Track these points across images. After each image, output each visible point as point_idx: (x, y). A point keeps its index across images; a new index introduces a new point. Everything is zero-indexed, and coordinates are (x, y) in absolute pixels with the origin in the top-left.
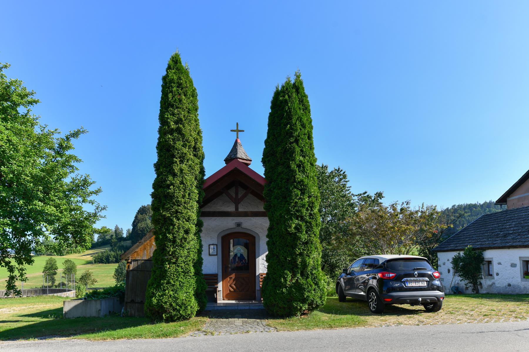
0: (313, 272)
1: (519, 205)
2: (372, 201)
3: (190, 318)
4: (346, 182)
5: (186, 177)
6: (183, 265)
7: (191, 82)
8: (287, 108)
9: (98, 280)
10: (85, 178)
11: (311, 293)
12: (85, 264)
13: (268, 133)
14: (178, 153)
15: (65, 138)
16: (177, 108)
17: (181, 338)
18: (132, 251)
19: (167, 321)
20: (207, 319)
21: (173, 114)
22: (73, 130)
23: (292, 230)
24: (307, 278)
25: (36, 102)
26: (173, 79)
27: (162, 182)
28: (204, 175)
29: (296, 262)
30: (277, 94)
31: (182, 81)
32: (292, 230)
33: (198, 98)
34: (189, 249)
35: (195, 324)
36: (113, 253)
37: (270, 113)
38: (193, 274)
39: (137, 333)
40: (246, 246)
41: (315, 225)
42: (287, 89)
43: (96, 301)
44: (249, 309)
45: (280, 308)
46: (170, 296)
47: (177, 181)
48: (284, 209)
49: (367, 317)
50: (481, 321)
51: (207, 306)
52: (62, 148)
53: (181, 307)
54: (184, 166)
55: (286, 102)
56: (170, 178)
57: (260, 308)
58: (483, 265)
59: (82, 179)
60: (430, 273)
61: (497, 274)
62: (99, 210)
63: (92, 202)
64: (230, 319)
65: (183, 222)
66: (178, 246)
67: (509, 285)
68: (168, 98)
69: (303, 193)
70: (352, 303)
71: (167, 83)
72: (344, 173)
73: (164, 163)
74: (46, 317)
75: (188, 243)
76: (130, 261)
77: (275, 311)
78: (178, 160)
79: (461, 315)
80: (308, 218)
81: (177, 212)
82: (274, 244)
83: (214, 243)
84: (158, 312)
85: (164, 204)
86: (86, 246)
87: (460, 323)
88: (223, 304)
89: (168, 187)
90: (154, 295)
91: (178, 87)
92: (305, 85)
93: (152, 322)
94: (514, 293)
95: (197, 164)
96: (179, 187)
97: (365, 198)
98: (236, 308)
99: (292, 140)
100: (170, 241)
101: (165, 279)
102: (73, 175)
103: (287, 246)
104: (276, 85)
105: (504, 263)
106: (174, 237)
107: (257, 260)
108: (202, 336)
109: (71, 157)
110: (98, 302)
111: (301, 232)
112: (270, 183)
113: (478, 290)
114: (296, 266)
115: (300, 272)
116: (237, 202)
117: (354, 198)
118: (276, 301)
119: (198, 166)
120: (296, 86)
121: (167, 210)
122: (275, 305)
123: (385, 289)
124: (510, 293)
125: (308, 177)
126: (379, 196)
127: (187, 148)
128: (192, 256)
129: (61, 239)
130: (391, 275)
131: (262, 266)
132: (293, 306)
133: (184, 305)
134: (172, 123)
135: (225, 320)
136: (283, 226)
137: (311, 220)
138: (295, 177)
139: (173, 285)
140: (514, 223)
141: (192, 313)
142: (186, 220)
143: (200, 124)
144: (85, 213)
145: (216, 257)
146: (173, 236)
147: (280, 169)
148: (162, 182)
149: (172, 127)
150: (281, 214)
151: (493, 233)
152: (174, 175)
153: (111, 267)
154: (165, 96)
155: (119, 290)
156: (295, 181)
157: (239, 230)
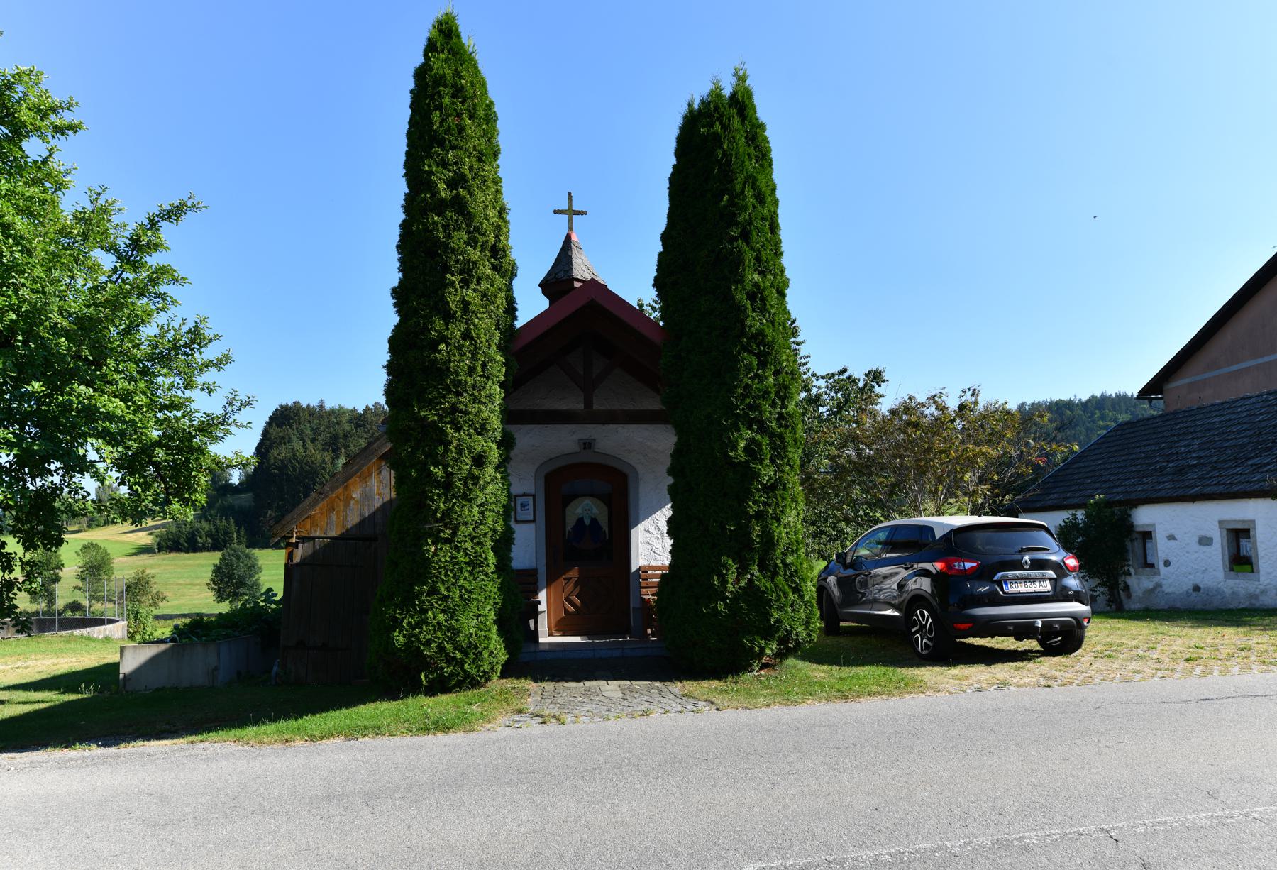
0: (789, 560)
1: (1209, 397)
2: (854, 392)
3: (487, 680)
4: (798, 344)
6: (469, 545)
7: (483, 85)
9: (167, 593)
10: (196, 327)
12: (133, 554)
14: (457, 261)
15: (146, 222)
16: (453, 148)
19: (432, 691)
21: (444, 164)
24: (775, 574)
25: (74, 128)
26: (443, 77)
28: (515, 318)
32: (739, 454)
33: (499, 125)
34: (482, 505)
35: (504, 698)
36: (205, 525)
37: (674, 167)
38: (493, 568)
39: (366, 723)
40: (607, 500)
41: (791, 442)
42: (717, 108)
46: (439, 624)
47: (456, 331)
50: (1187, 674)
52: (136, 248)
53: (466, 654)
54: (470, 294)
55: (716, 139)
56: (439, 324)
58: (1132, 541)
59: (185, 329)
60: (1054, 558)
61: (1167, 563)
63: (209, 389)
64: (587, 683)
65: (470, 436)
67: (1197, 588)
68: (431, 123)
69: (763, 365)
74: (75, 690)
75: (482, 489)
76: (294, 540)
78: (456, 279)
79: (1126, 661)
81: (454, 409)
83: (528, 492)
86: (193, 502)
87: (1143, 679)
88: (550, 644)
90: (397, 624)
92: (757, 100)
94: (1208, 607)
96: (459, 348)
97: (841, 381)
99: (735, 232)
100: (437, 483)
101: (425, 583)
102: (162, 319)
104: (689, 98)
105: (1182, 535)
106: (449, 475)
107: (633, 531)
108: (534, 728)
109: (162, 271)
111: (761, 461)
113: (1121, 602)
117: (816, 383)
119: (503, 295)
121: (431, 404)
124: (1199, 606)
127: (479, 248)
128: (490, 521)
129: (136, 483)
130: (968, 565)
131: (651, 545)
134: (442, 186)
135: (573, 685)
138: (743, 325)
139: (446, 598)
140: (1197, 442)
141: (492, 668)
142: (476, 430)
145: (532, 525)
149: (443, 194)
151: (1149, 465)
152: (448, 317)
153: (202, 562)
156: (742, 333)
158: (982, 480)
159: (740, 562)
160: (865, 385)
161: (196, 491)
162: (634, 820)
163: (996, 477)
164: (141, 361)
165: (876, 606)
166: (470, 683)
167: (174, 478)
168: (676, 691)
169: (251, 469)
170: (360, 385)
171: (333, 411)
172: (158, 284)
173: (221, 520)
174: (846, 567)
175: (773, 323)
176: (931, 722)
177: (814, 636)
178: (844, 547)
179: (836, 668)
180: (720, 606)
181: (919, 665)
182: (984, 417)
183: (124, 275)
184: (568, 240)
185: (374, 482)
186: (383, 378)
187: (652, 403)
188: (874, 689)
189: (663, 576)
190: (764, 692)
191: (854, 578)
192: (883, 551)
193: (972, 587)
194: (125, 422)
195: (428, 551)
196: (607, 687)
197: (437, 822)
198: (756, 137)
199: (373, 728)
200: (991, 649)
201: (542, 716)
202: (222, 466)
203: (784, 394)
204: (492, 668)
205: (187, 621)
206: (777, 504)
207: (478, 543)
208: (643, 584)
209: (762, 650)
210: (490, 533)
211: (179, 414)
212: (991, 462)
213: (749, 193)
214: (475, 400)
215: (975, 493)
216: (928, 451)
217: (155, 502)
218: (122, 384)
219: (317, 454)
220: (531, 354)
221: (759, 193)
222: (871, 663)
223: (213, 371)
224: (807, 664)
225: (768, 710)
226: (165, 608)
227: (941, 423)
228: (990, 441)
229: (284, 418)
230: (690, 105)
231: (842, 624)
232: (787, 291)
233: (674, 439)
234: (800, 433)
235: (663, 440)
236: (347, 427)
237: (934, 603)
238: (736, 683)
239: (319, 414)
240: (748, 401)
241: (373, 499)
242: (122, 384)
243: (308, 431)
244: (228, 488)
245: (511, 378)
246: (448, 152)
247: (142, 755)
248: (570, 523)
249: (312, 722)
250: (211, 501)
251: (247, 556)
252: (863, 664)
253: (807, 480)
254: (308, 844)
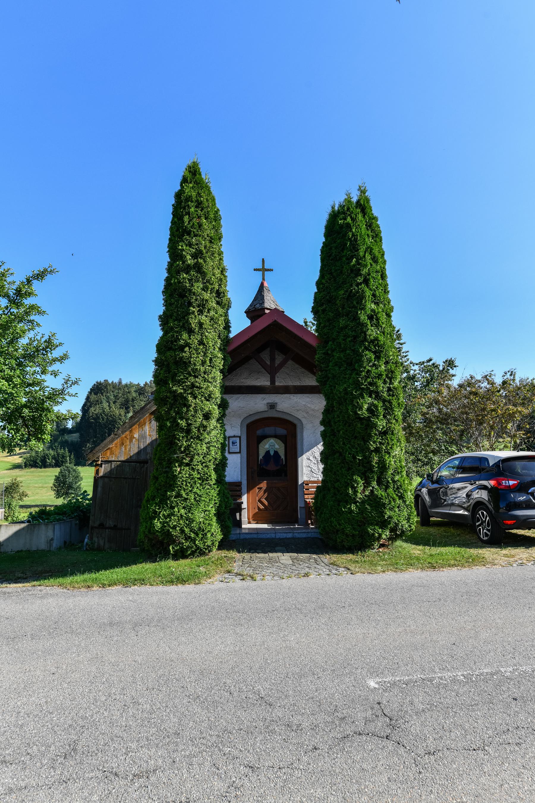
2: (436, 374)
3: (209, 551)
4: (401, 344)
5: (207, 334)
6: (200, 467)
7: (213, 200)
8: (350, 234)
9: (29, 493)
10: (49, 339)
11: (395, 511)
13: (322, 270)
14: (196, 300)
15: (25, 280)
16: (195, 236)
17: (205, 586)
18: (103, 448)
20: (233, 554)
21: (190, 245)
22: (38, 268)
23: (364, 412)
24: (387, 487)
26: (190, 196)
27: (172, 342)
28: (229, 332)
29: (370, 462)
30: (334, 216)
31: (202, 199)
33: (222, 222)
34: (208, 443)
35: (219, 562)
36: (52, 452)
37: (324, 243)
38: (214, 482)
39: (136, 577)
42: (348, 209)
43: (46, 525)
44: (293, 538)
45: (347, 536)
46: (181, 516)
47: (194, 340)
48: (351, 381)
49: (480, 551)
51: (232, 532)
55: (348, 226)
56: (185, 336)
57: (309, 535)
62: (69, 385)
63: (55, 374)
64: (271, 555)
65: (202, 401)
66: (194, 439)
69: (378, 358)
70: (442, 529)
71: (182, 201)
72: (398, 331)
73: (175, 314)
75: (208, 434)
76: (100, 462)
77: (338, 540)
78: (196, 310)
80: (385, 394)
81: (193, 386)
82: (334, 435)
83: (237, 435)
84: (162, 543)
85: (175, 375)
88: (249, 529)
89: (182, 349)
90: (156, 515)
91: (196, 207)
92: (372, 203)
93: (152, 558)
95: (221, 315)
96: (197, 350)
97: (429, 367)
98: (273, 536)
99: (360, 280)
101: (173, 490)
102: (31, 334)
103: (356, 437)
104: (332, 203)
106: (189, 425)
107: (300, 459)
108: (237, 583)
109: (32, 307)
110: (50, 527)
112: (327, 342)
114: (370, 469)
115: (376, 478)
116: (272, 371)
118: (340, 525)
120: (361, 205)
121: (180, 383)
122: (338, 531)
123: (502, 505)
125: (384, 334)
126: (449, 364)
127: (209, 292)
128: (213, 453)
129: (11, 429)
130: (511, 483)
131: (310, 468)
132: (368, 532)
133: (201, 532)
134: (189, 257)
135: (262, 555)
136: (350, 407)
137: (391, 398)
138: (365, 334)
141: (213, 544)
142: (205, 398)
143: (224, 259)
144: (48, 389)
145: (239, 455)
146: (187, 423)
147: (342, 322)
148: (172, 342)
149: (189, 262)
150: (345, 389)
152: (191, 331)
153: (49, 474)
154: (179, 219)
155: (79, 507)
156: (365, 339)
157: (272, 414)
158: (519, 428)
159: (365, 479)
160: (444, 369)
161: (45, 433)
162: (297, 646)
163: (528, 426)
164: (18, 358)
165: (453, 508)
166: (199, 553)
167: (34, 426)
168: (326, 561)
169: (79, 419)
170: (139, 371)
171: (126, 385)
172: (29, 315)
173: (61, 449)
174: (433, 482)
175: (384, 333)
176: (490, 586)
177: (413, 527)
178: (432, 469)
179: (427, 548)
180: (353, 507)
181: (481, 547)
182: (519, 389)
183: (12, 310)
184: (262, 286)
185: (147, 428)
186: (152, 367)
187: (311, 381)
188: (452, 562)
189: (318, 487)
190: (381, 563)
191: (438, 490)
192: (456, 472)
193: (515, 497)
194: (7, 394)
195: (176, 471)
196: (283, 558)
197: (175, 643)
198: (372, 225)
199: (140, 580)
200: (529, 537)
201: (242, 575)
202: (61, 419)
203: (391, 376)
204: (213, 544)
205: (37, 509)
206: (388, 443)
207: (206, 466)
208: (306, 492)
209: (380, 535)
210: (213, 460)
211: (38, 389)
212: (524, 417)
213: (368, 257)
214: (205, 380)
215: (515, 436)
216: (484, 409)
217: (21, 440)
218: (7, 372)
219: (117, 411)
220: (238, 355)
221: (374, 257)
222: (450, 545)
223: (58, 363)
224: (409, 545)
225: (384, 575)
226: (27, 501)
227: (491, 393)
228: (523, 403)
229: (98, 389)
230: (333, 208)
231: (432, 519)
232: (392, 314)
233: (325, 403)
234: (401, 399)
235: (316, 404)
236: (134, 395)
237: (490, 506)
238: (364, 556)
239: (118, 387)
240: (369, 380)
241: (146, 438)
242: (7, 372)
243: (112, 397)
244: (65, 431)
245: (227, 367)
246: (192, 238)
247: (5, 593)
248: (262, 454)
249: (105, 575)
250: (54, 438)
251: (74, 470)
252: (445, 546)
253: (408, 429)
254: (97, 654)
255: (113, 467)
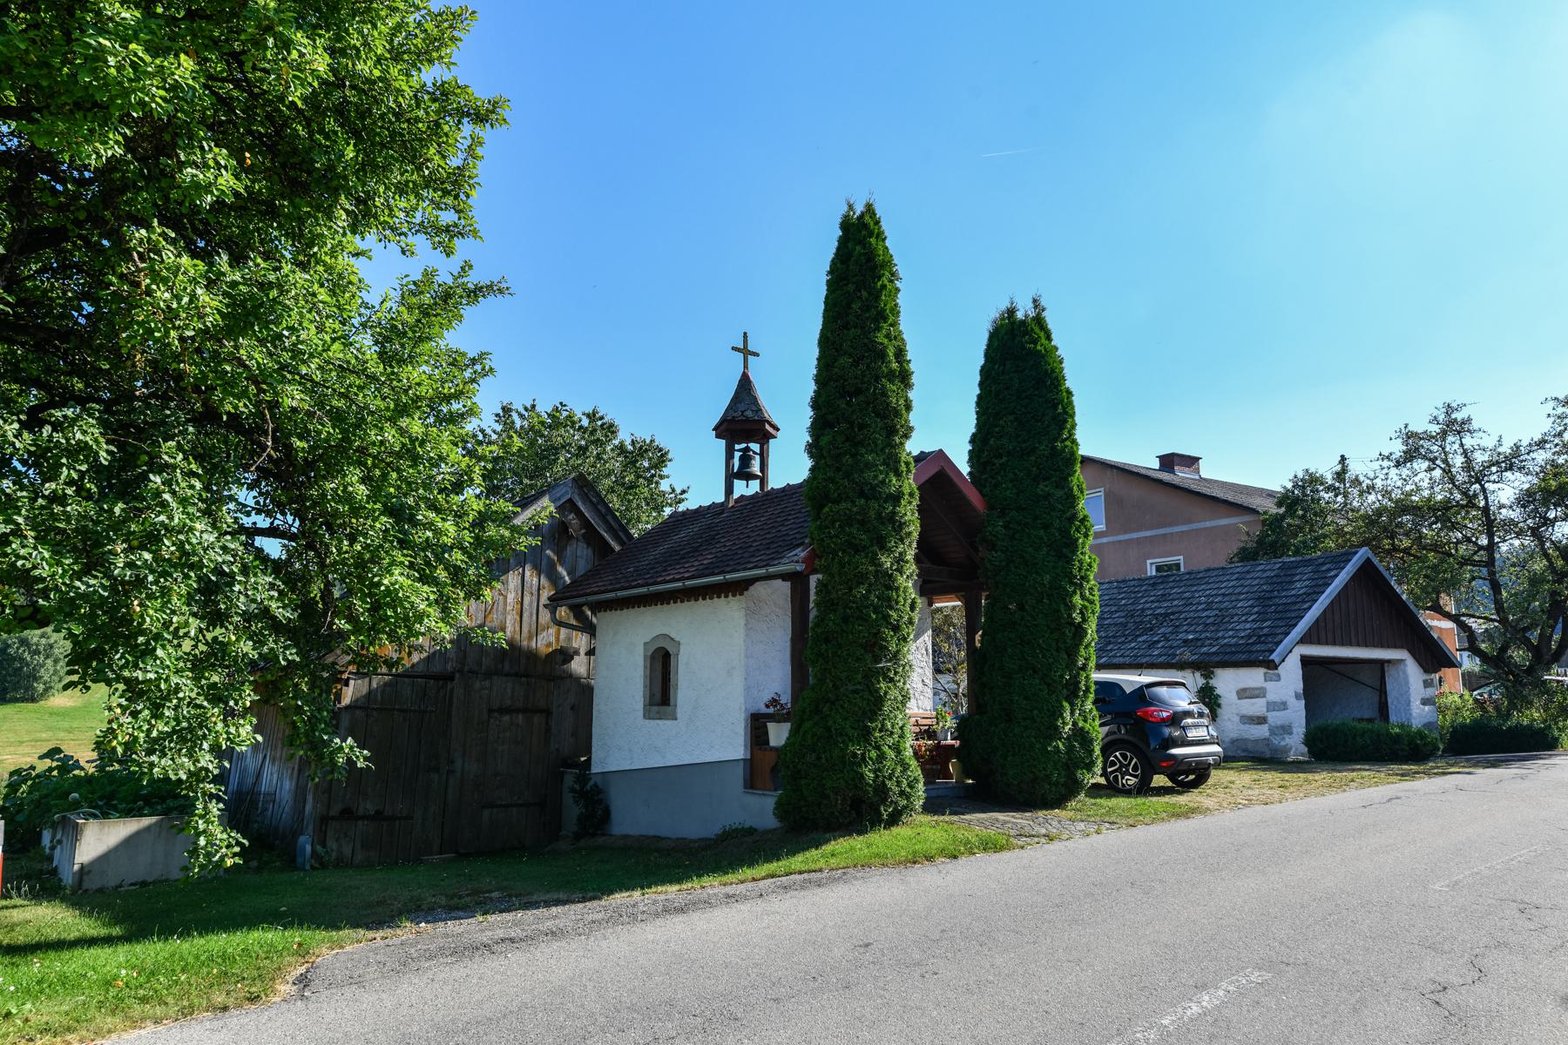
255: (374, 685)
